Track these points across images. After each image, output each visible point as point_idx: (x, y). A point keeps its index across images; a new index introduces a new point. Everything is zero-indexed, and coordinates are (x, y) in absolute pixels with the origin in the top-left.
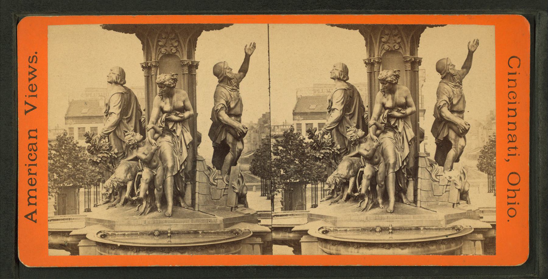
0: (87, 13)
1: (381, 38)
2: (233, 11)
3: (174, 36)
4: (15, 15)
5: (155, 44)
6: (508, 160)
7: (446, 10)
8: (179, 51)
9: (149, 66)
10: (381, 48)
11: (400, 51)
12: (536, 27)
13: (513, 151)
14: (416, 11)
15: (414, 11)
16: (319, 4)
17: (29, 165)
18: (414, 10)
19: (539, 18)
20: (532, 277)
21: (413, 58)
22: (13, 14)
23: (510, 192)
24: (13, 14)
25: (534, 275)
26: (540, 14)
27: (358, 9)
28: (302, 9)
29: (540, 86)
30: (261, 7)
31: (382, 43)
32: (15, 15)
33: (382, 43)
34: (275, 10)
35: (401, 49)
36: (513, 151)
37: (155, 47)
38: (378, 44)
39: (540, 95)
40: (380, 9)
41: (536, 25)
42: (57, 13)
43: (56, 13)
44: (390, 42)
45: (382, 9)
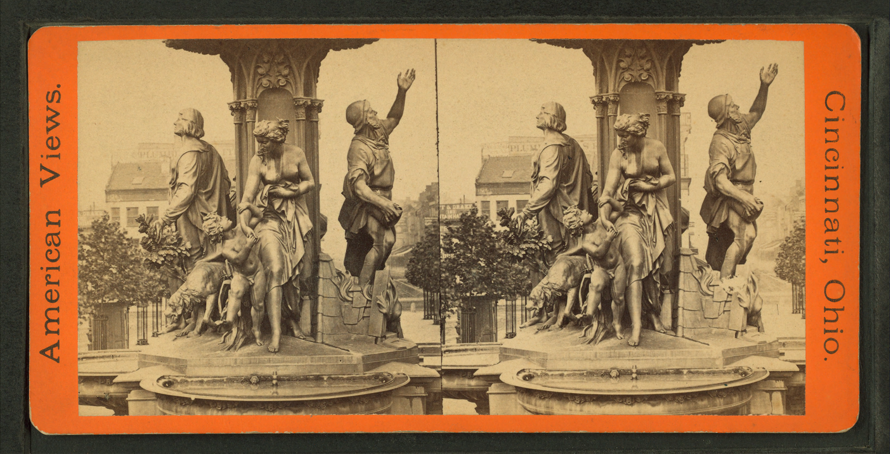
0: (141, 21)
1: (619, 61)
2: (378, 18)
3: (283, 59)
4: (24, 25)
5: (252, 72)
6: (826, 261)
7: (724, 17)
8: (290, 84)
9: (242, 108)
10: (619, 78)
11: (288, 88)
12: (871, 45)
13: (833, 246)
14: (676, 17)
15: (673, 18)
16: (518, 6)
17: (48, 269)
18: (671, 16)
19: (876, 30)
20: (865, 451)
21: (671, 95)
22: (21, 22)
23: (828, 170)
24: (21, 22)
25: (868, 447)
26: (876, 22)
27: (581, 15)
28: (490, 16)
29: (876, 141)
30: (424, 11)
31: (621, 71)
32: (24, 25)
33: (621, 71)
34: (447, 16)
35: (651, 79)
36: (833, 246)
37: (251, 77)
38: (613, 71)
39: (877, 155)
40: (617, 15)
41: (871, 41)
42: (93, 21)
43: (90, 21)
44: (633, 68)
45: (620, 15)
